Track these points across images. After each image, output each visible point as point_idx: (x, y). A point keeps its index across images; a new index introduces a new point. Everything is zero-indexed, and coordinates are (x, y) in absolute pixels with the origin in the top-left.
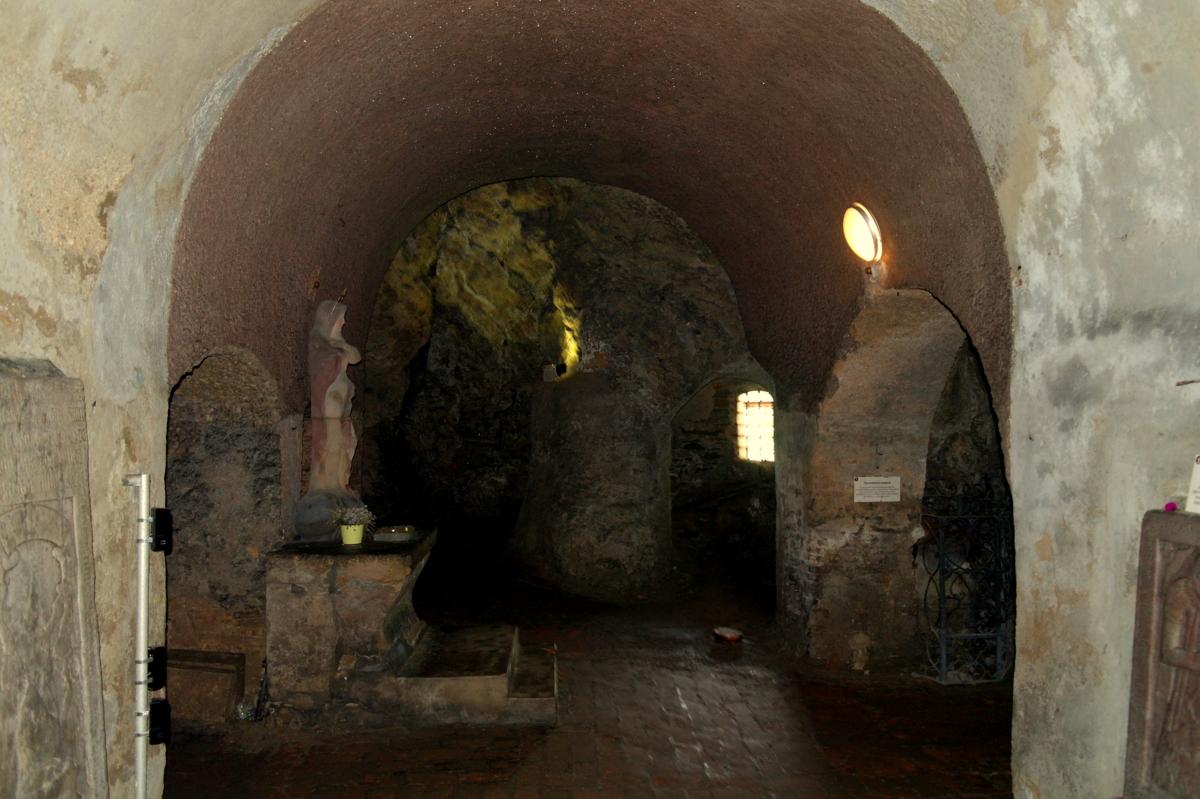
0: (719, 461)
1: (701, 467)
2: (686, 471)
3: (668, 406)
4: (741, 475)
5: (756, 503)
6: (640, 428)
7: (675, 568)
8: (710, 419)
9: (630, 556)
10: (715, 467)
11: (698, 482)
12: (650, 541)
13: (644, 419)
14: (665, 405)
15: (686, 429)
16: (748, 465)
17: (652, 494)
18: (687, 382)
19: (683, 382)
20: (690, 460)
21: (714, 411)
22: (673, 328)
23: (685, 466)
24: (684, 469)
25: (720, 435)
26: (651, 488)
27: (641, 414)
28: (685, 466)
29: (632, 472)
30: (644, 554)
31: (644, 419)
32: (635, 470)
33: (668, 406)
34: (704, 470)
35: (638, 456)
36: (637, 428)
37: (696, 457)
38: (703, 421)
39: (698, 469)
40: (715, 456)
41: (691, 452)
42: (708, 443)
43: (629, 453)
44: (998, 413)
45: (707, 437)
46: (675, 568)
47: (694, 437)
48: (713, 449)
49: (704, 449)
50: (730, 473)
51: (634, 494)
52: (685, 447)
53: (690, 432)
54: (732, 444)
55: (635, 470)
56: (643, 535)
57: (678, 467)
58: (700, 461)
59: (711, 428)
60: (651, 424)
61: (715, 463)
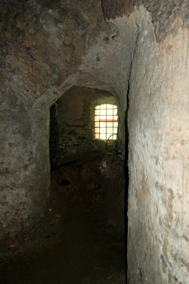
0: (85, 140)
1: (76, 144)
2: (69, 145)
3: (38, 93)
4: (96, 148)
5: (104, 165)
6: (16, 111)
7: (50, 210)
8: (81, 119)
9: (6, 213)
10: (83, 144)
11: (74, 151)
12: (24, 199)
13: (19, 103)
14: (35, 92)
15: (69, 124)
16: (99, 142)
17: (28, 163)
18: (54, 72)
19: (50, 72)
20: (71, 140)
21: (83, 114)
22: (37, 16)
23: (68, 143)
24: (67, 144)
25: (86, 127)
26: (27, 158)
27: (17, 99)
28: (68, 143)
29: (8, 146)
30: (19, 210)
31: (19, 103)
32: (10, 145)
33: (38, 93)
34: (77, 145)
35: (14, 133)
36: (12, 110)
37: (73, 138)
38: (77, 120)
39: (75, 145)
40: (83, 138)
41: (71, 136)
42: (79, 131)
43: (5, 129)
44: (46, 144)
45: (79, 128)
46: (50, 210)
47: (73, 128)
48: (82, 135)
49: (78, 134)
50: (90, 147)
51: (10, 164)
52: (68, 133)
53: (70, 126)
54: (92, 132)
55: (10, 145)
56: (18, 195)
57: (64, 143)
58: (76, 141)
59: (81, 124)
60: (26, 108)
61: (83, 142)
